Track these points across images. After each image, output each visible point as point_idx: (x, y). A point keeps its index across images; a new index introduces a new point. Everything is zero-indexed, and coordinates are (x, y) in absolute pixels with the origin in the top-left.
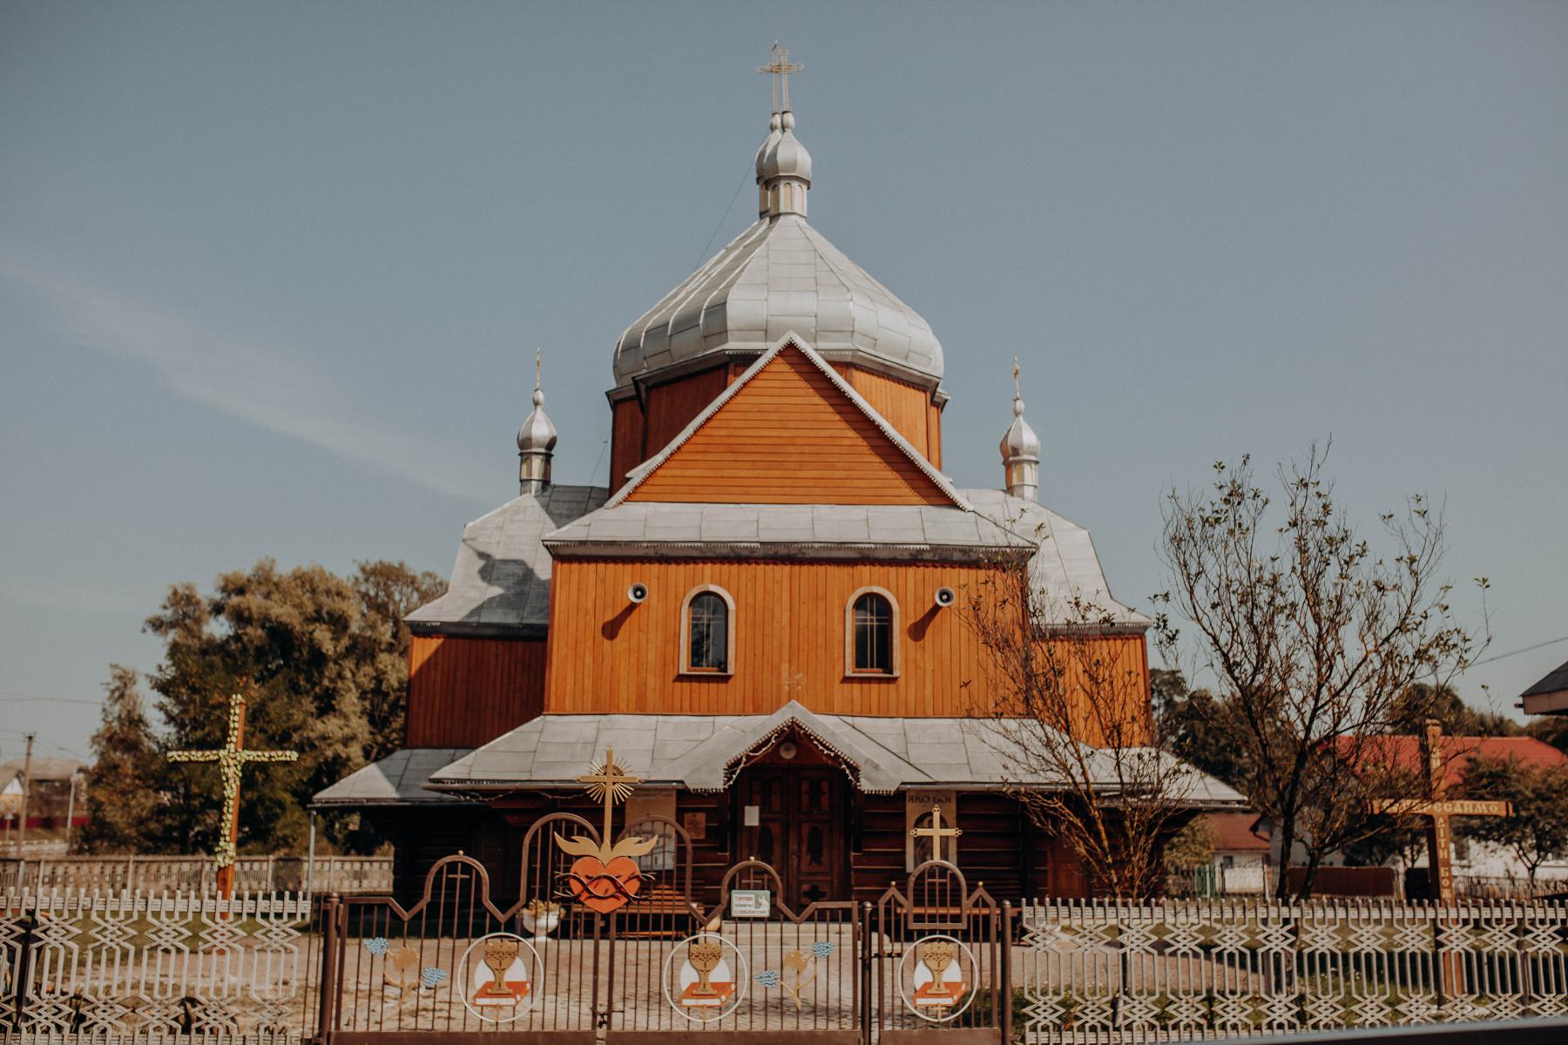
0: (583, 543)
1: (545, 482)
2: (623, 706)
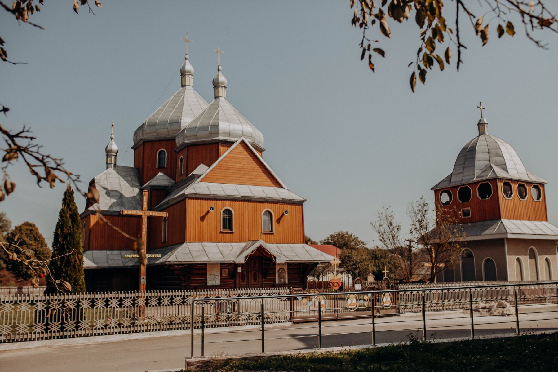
0: (196, 194)
1: (115, 164)
2: (206, 239)
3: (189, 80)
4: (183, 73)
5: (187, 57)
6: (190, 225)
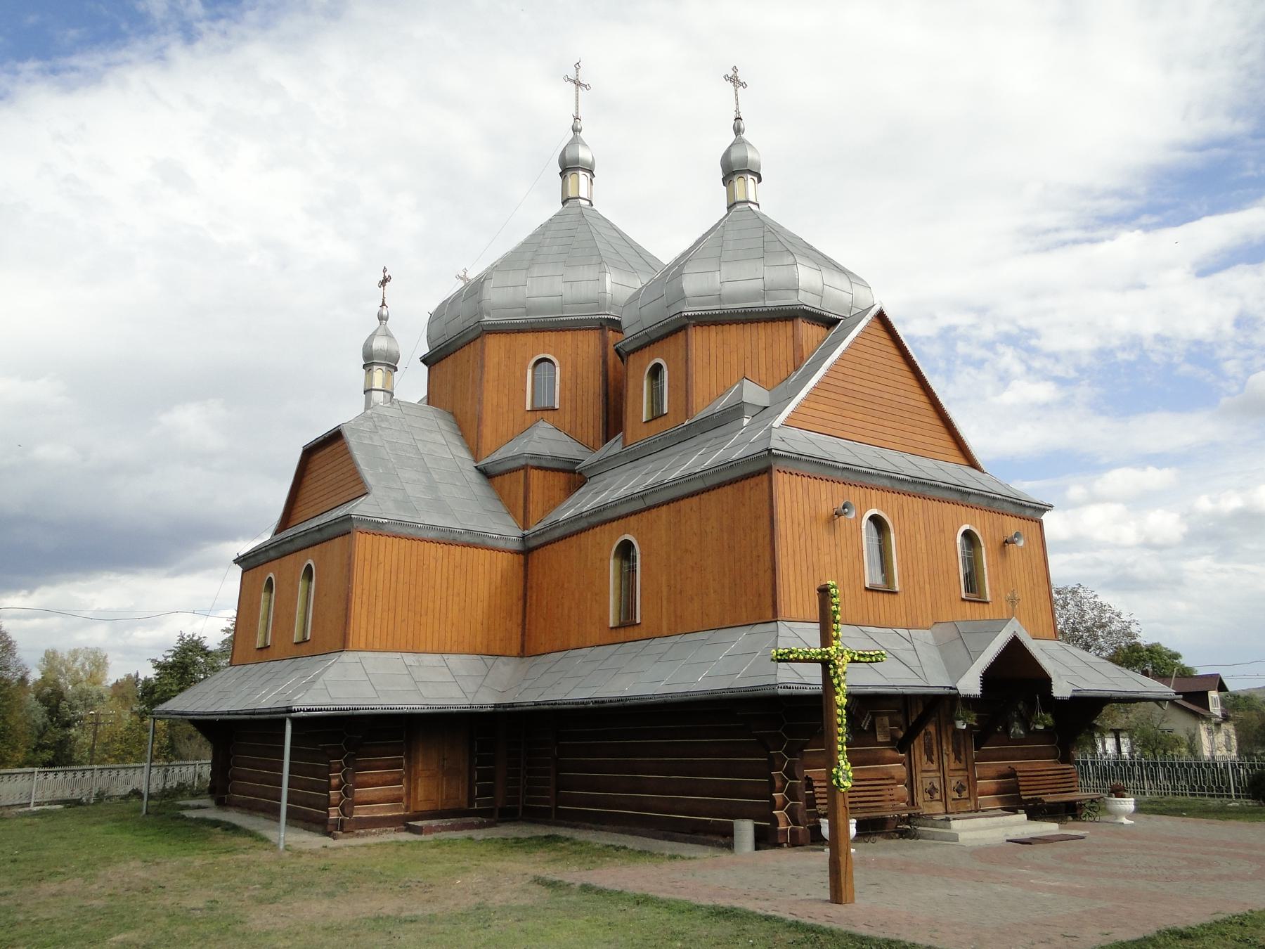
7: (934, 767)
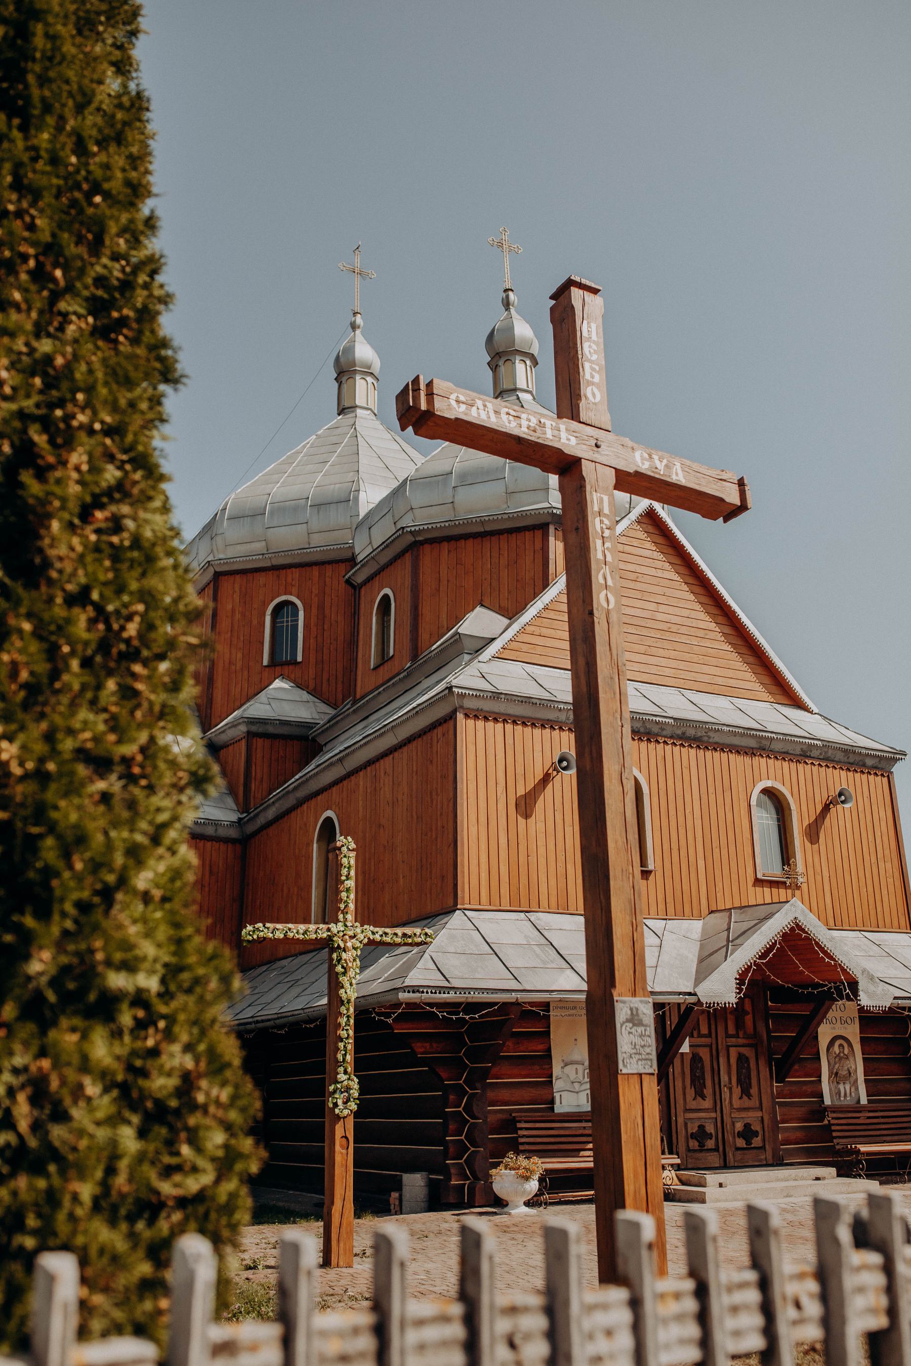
3: (363, 391)
4: (345, 371)
5: (359, 320)
6: (473, 830)
7: (707, 1104)
